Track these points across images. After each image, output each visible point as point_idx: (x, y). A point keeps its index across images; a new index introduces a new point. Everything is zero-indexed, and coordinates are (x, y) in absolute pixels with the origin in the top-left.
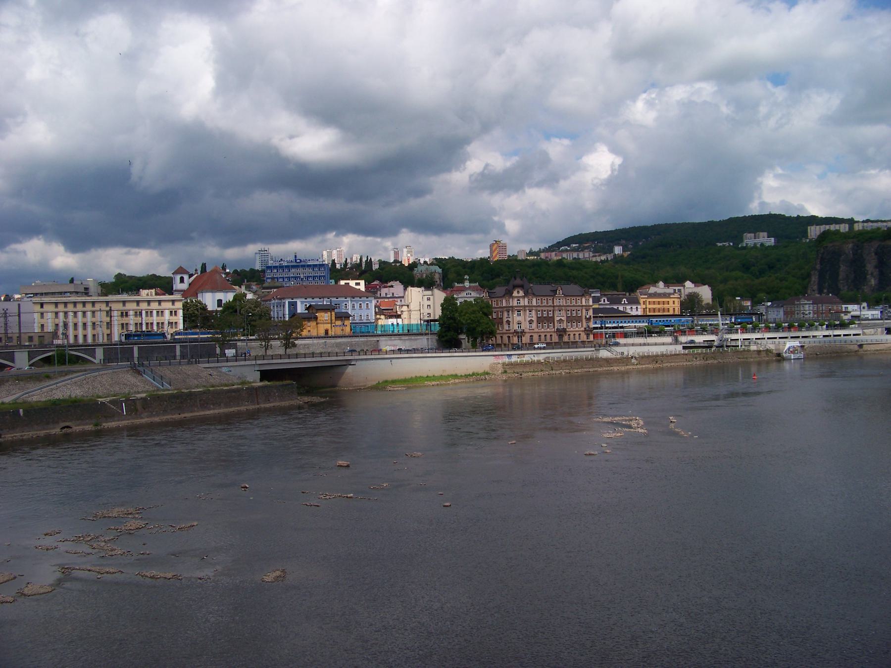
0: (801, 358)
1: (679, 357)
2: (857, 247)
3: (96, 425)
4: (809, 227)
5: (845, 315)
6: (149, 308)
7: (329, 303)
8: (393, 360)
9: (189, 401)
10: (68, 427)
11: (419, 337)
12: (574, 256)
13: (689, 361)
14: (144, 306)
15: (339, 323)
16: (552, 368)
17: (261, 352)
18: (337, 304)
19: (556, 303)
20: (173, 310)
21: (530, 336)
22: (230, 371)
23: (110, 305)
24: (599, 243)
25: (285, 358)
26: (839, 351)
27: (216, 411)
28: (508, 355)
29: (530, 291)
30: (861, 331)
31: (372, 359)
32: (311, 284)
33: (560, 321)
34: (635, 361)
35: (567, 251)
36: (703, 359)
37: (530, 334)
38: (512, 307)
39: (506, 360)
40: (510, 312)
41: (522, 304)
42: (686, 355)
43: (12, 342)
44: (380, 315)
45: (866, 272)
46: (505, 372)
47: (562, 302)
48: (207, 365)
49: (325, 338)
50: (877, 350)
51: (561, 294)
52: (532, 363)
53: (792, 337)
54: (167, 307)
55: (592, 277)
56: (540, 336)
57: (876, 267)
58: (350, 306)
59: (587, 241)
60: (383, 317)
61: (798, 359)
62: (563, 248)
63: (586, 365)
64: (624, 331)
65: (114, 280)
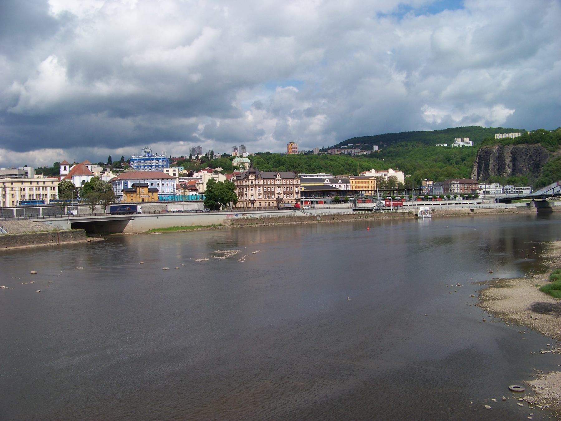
0: (430, 217)
1: (349, 216)
2: (501, 148)
4: (496, 135)
5: (479, 191)
6: (38, 185)
8: (158, 217)
9: (13, 240)
11: (192, 203)
12: (349, 152)
13: (356, 219)
14: (34, 184)
16: (263, 222)
17: (91, 212)
19: (277, 182)
21: (259, 203)
22: (52, 223)
23: (5, 184)
24: (366, 143)
26: (458, 213)
27: (30, 246)
28: (235, 214)
29: (259, 175)
30: (482, 201)
31: (145, 216)
32: (150, 170)
33: (279, 194)
34: (320, 218)
35: (345, 148)
36: (365, 217)
37: (259, 202)
38: (248, 185)
39: (234, 217)
40: (247, 188)
41: (254, 184)
42: (354, 214)
44: (186, 190)
45: (505, 164)
46: (233, 224)
47: (281, 182)
49: (142, 203)
50: (483, 213)
51: (280, 177)
52: (251, 219)
53: (426, 205)
54: (49, 185)
55: (343, 166)
56: (266, 203)
57: (511, 161)
58: (161, 184)
59: (358, 142)
60: (187, 190)
61: (427, 218)
62: (343, 146)
63: (286, 220)
64: (321, 200)
65: (53, 167)
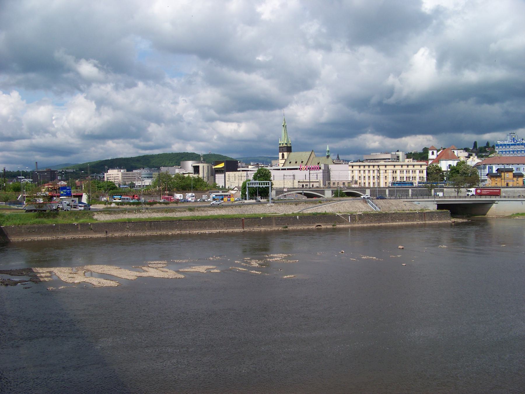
3: (333, 226)
7: (503, 168)
8: (523, 202)
10: (320, 226)
15: (515, 179)
18: (518, 168)
20: (395, 170)
22: (419, 204)
25: (458, 198)
43: (335, 185)
48: (406, 200)
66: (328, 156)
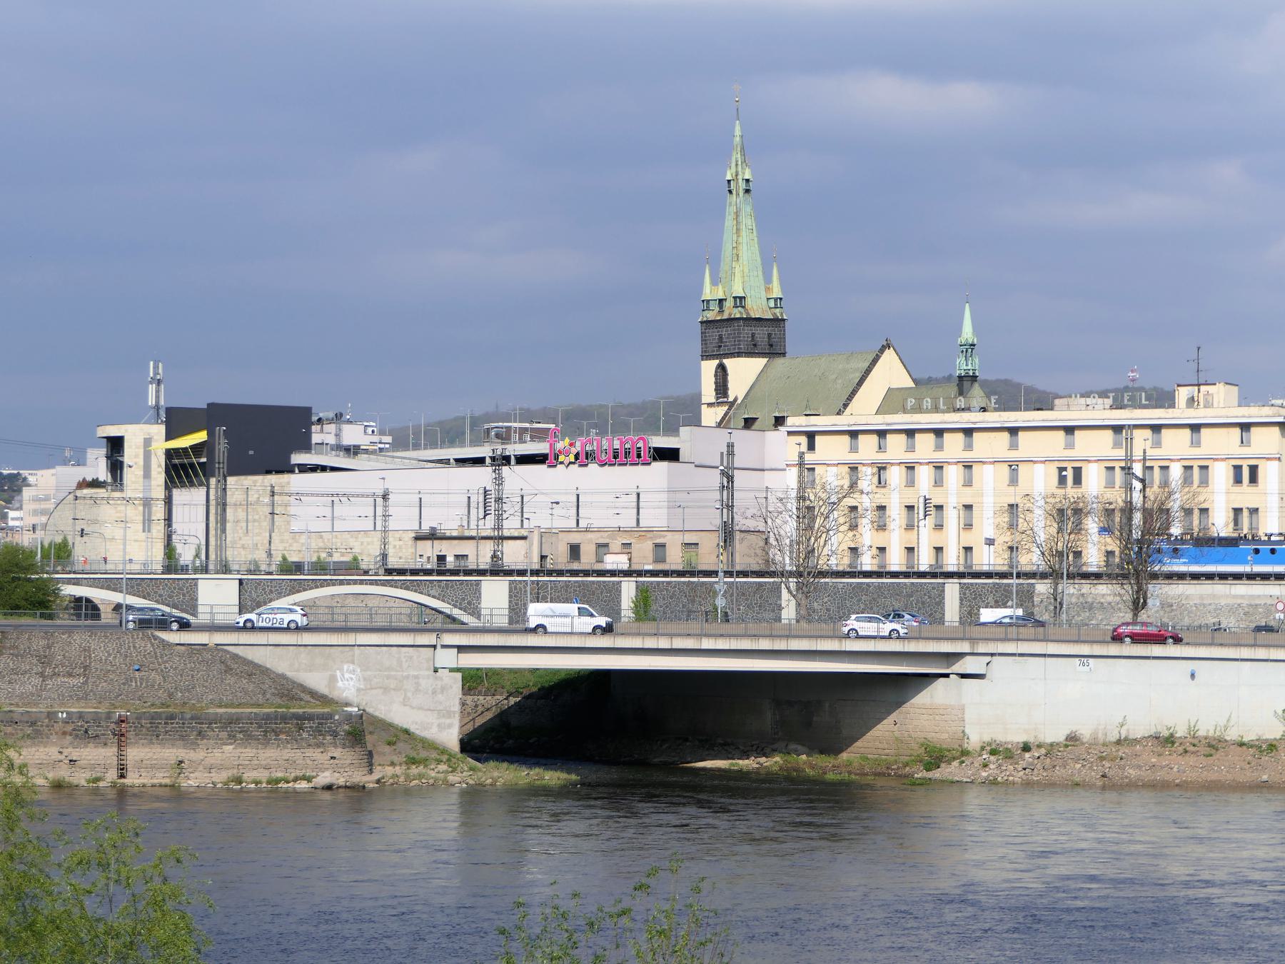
66: (967, 376)
